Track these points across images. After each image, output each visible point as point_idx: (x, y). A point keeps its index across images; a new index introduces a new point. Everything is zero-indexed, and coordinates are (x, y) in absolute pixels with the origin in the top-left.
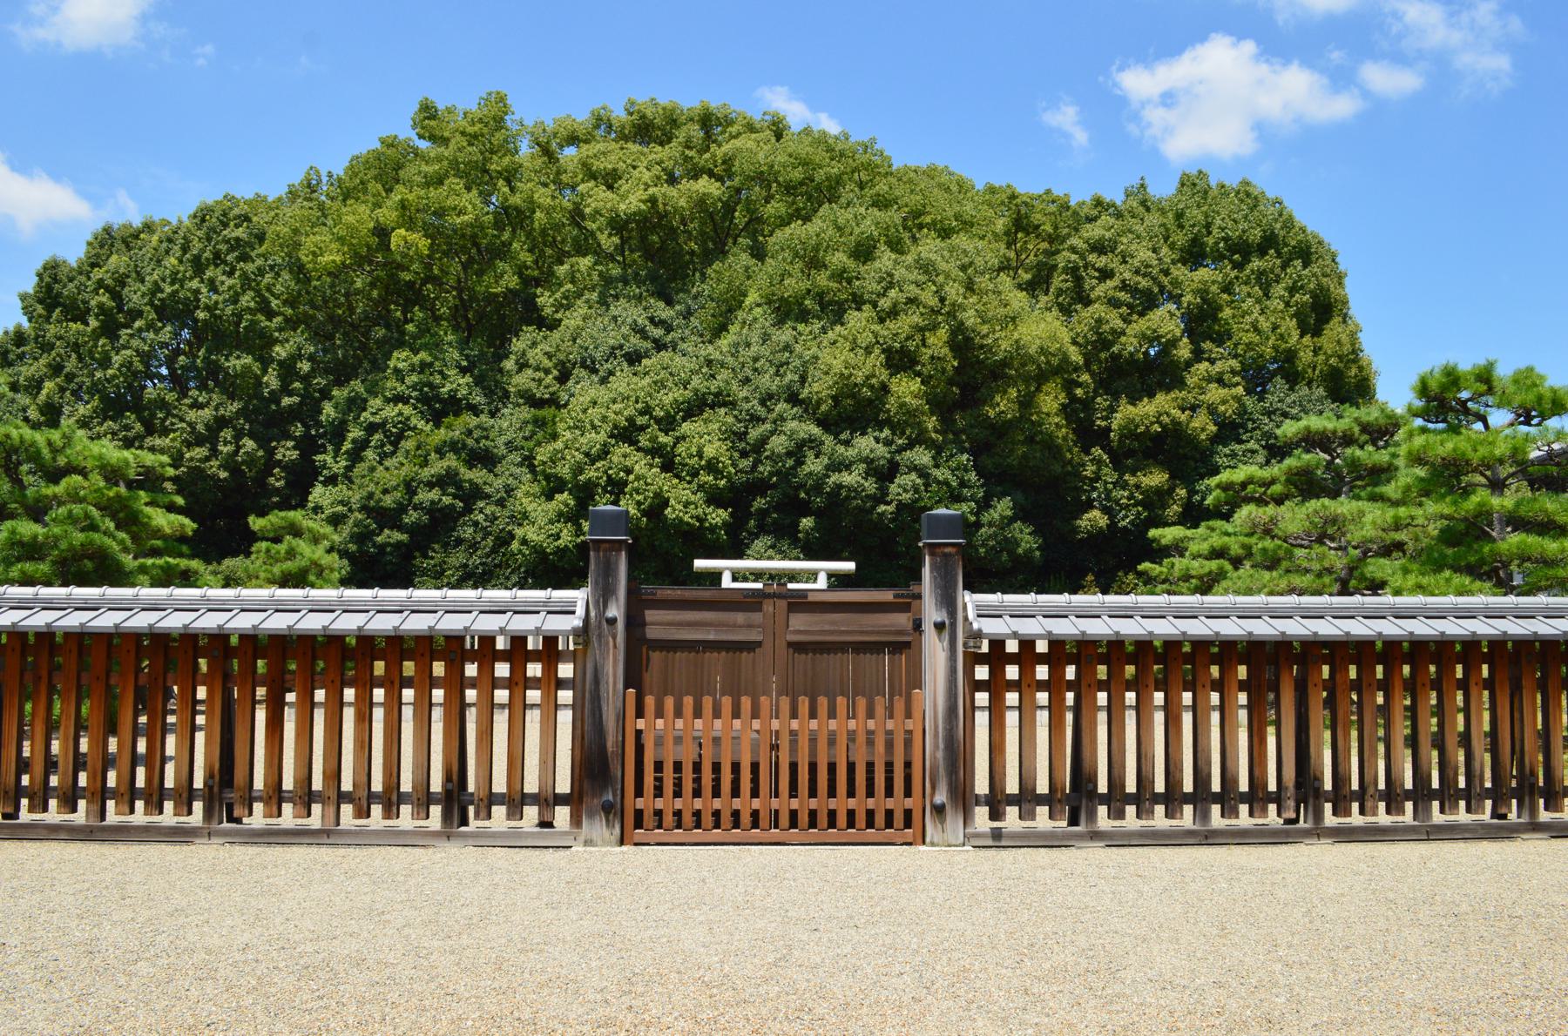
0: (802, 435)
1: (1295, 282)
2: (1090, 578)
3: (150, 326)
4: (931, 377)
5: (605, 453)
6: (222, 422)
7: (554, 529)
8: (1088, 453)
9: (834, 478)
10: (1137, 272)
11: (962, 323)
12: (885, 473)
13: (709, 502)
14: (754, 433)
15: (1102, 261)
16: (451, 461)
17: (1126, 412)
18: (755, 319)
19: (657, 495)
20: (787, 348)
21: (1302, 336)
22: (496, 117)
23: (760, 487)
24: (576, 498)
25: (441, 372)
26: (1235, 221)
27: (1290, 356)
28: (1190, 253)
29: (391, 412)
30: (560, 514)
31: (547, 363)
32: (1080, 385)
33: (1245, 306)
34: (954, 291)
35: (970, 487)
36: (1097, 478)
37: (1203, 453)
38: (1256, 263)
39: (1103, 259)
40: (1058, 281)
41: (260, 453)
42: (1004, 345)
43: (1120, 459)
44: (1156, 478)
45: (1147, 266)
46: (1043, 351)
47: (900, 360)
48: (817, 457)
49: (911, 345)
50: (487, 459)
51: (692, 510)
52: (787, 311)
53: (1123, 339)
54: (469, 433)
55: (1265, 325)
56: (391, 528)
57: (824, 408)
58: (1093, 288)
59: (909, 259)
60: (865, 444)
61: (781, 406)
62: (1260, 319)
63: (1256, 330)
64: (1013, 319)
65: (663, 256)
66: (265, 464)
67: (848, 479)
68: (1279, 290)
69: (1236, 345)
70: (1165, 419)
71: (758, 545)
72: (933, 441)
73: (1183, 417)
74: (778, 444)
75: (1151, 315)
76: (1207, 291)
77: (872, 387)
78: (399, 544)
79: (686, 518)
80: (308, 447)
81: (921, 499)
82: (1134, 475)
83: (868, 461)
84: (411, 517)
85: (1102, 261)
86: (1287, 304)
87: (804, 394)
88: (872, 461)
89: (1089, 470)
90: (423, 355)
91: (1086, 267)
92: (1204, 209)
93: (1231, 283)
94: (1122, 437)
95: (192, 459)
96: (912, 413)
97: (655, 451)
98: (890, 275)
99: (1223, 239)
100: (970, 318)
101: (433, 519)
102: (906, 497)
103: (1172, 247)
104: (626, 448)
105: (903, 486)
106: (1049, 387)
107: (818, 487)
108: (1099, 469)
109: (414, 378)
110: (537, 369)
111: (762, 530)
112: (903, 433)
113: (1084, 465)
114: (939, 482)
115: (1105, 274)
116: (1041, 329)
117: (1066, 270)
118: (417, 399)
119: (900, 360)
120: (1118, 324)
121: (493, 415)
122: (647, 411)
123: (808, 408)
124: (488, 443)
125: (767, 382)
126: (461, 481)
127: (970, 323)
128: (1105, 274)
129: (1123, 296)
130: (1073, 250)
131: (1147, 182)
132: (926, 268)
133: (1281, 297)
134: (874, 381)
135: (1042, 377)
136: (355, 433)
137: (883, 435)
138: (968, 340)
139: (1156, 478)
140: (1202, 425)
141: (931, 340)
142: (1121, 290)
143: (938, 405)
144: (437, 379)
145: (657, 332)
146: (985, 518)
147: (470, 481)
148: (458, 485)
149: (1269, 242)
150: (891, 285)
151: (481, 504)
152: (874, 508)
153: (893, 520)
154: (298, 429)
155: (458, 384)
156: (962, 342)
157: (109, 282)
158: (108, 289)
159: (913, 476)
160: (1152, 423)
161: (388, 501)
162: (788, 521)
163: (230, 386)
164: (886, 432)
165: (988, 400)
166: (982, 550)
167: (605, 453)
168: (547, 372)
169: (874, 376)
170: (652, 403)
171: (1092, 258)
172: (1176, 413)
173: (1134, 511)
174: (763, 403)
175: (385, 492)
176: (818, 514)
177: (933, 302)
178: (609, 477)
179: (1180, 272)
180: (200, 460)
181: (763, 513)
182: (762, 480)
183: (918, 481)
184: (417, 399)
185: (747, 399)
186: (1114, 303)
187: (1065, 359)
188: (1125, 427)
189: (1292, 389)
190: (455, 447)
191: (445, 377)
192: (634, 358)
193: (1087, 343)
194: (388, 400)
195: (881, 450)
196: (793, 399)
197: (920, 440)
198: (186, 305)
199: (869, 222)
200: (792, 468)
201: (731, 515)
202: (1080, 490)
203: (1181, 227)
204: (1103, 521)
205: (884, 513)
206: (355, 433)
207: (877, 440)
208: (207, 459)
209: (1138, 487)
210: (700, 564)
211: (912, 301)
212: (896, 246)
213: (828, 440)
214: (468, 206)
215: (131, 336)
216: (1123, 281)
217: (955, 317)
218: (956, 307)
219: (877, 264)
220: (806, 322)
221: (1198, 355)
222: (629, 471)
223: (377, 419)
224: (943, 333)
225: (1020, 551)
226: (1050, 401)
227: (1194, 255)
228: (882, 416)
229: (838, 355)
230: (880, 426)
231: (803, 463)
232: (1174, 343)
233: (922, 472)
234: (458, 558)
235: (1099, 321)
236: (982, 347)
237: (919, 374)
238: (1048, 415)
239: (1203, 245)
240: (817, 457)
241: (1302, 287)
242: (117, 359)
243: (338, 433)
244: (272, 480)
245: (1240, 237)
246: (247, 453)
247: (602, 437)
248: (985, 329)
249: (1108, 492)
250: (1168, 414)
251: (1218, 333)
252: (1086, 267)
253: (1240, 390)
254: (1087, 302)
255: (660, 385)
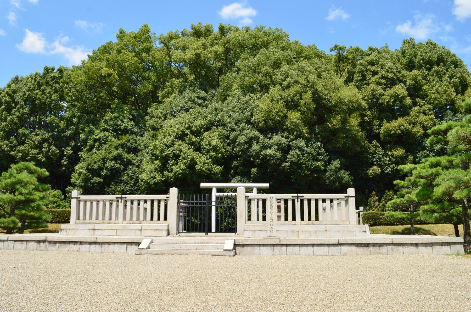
0: (251, 135)
1: (452, 74)
2: (374, 193)
3: (22, 107)
4: (305, 112)
5: (173, 144)
6: (44, 140)
7: (153, 175)
8: (371, 143)
9: (264, 152)
10: (388, 71)
11: (317, 90)
12: (285, 150)
13: (213, 163)
14: (232, 136)
15: (373, 68)
16: (120, 151)
17: (387, 126)
18: (236, 94)
19: (192, 159)
20: (247, 103)
21: (457, 95)
22: (146, 30)
23: (235, 157)
24: (162, 163)
25: (122, 120)
26: (427, 53)
27: (452, 103)
28: (408, 66)
29: (102, 135)
30: (156, 169)
31: (160, 115)
32: (366, 116)
33: (432, 84)
34: (313, 78)
35: (321, 155)
36: (375, 153)
37: (419, 141)
38: (435, 68)
39: (374, 68)
40: (356, 77)
41: (58, 151)
42: (334, 98)
43: (384, 145)
44: (400, 152)
45: (392, 69)
46: (350, 101)
47: (291, 105)
48: (257, 144)
49: (296, 99)
50: (135, 150)
51: (206, 166)
52: (248, 89)
53: (383, 97)
54: (129, 141)
55: (441, 90)
56: (97, 177)
57: (260, 124)
58: (370, 79)
59: (295, 67)
60: (277, 138)
61: (243, 125)
62: (439, 88)
63: (438, 93)
64: (338, 89)
65: (206, 76)
66: (60, 156)
67: (269, 152)
68: (446, 78)
69: (430, 99)
70: (402, 128)
71: (234, 179)
72: (306, 137)
73: (410, 127)
74: (241, 139)
75: (394, 87)
76: (416, 79)
77: (279, 116)
78: (99, 183)
79: (204, 169)
80: (77, 149)
81: (300, 160)
82: (391, 151)
83: (279, 145)
84: (104, 172)
85: (373, 68)
86: (450, 83)
87: (252, 120)
88: (280, 144)
89: (372, 150)
90: (116, 115)
91: (367, 71)
92: (414, 50)
93: (426, 76)
94: (385, 136)
95: (32, 154)
96: (296, 126)
97: (192, 144)
98: (287, 72)
99: (422, 59)
100: (319, 87)
101: (111, 173)
102: (294, 159)
103: (401, 64)
104: (180, 142)
105: (293, 155)
106: (354, 115)
107: (257, 156)
108: (376, 149)
109: (111, 122)
110: (157, 117)
111: (236, 174)
112: (293, 134)
113: (369, 148)
114: (308, 153)
115: (375, 73)
116: (350, 93)
117: (359, 72)
118: (112, 130)
119: (291, 105)
120: (381, 91)
121: (141, 136)
122: (189, 128)
123: (254, 125)
124: (136, 145)
125: (237, 115)
126: (123, 158)
127: (319, 90)
128: (375, 73)
129: (382, 81)
130: (361, 65)
131: (388, 45)
132: (301, 70)
133: (447, 80)
134: (280, 114)
135: (351, 111)
136: (90, 143)
137: (285, 135)
138: (319, 96)
139: (400, 152)
140: (418, 130)
141: (304, 96)
142: (381, 79)
143: (307, 122)
144: (120, 122)
145: (200, 101)
146: (329, 168)
147: (126, 158)
148: (122, 160)
149: (441, 60)
150: (287, 76)
151: (131, 167)
152: (281, 164)
153: (289, 169)
154: (73, 143)
155: (129, 124)
156: (317, 97)
157: (10, 92)
158: (9, 95)
159: (297, 151)
160: (397, 130)
161: (96, 166)
162: (246, 170)
163: (48, 127)
164: (286, 134)
165: (329, 120)
166: (327, 181)
167: (173, 144)
168: (160, 118)
169: (281, 111)
170: (191, 125)
171: (369, 67)
172: (407, 125)
173: (391, 166)
174: (236, 124)
175: (95, 163)
176: (259, 166)
177: (305, 82)
178: (174, 153)
179: (404, 72)
180: (35, 154)
181: (237, 167)
182: (236, 154)
183: (299, 153)
184: (112, 130)
185: (230, 122)
186: (379, 83)
187: (360, 105)
188: (386, 131)
189: (454, 115)
190: (123, 146)
191: (123, 122)
192: (187, 110)
193: (369, 99)
194: (101, 131)
195: (284, 141)
196: (248, 122)
197: (300, 136)
198: (33, 99)
199: (279, 54)
200: (247, 148)
201: (223, 168)
202: (367, 158)
203: (405, 57)
204: (378, 171)
205: (285, 166)
206: (90, 143)
207: (282, 137)
208: (38, 154)
209: (392, 156)
210: (203, 185)
211: (296, 82)
212: (289, 62)
213: (262, 137)
214: (129, 59)
215: (16, 111)
216: (382, 75)
217: (314, 88)
218: (314, 83)
219: (281, 69)
220: (254, 93)
221: (415, 104)
222: (181, 151)
223: (97, 138)
224: (309, 94)
225: (344, 181)
226: (354, 121)
227: (410, 66)
228: (285, 127)
229: (264, 104)
230: (283, 131)
231: (251, 146)
232: (404, 98)
233: (300, 149)
234: (121, 187)
235: (373, 90)
236: (325, 99)
237: (300, 110)
238: (354, 126)
239: (414, 63)
240: (257, 144)
241: (455, 76)
242: (9, 118)
243: (85, 142)
244: (63, 161)
245: (429, 58)
246: (53, 151)
247: (171, 138)
248: (326, 92)
249: (380, 158)
250: (403, 126)
251: (422, 95)
252: (367, 71)
253: (433, 116)
254: (368, 84)
255: (195, 119)
